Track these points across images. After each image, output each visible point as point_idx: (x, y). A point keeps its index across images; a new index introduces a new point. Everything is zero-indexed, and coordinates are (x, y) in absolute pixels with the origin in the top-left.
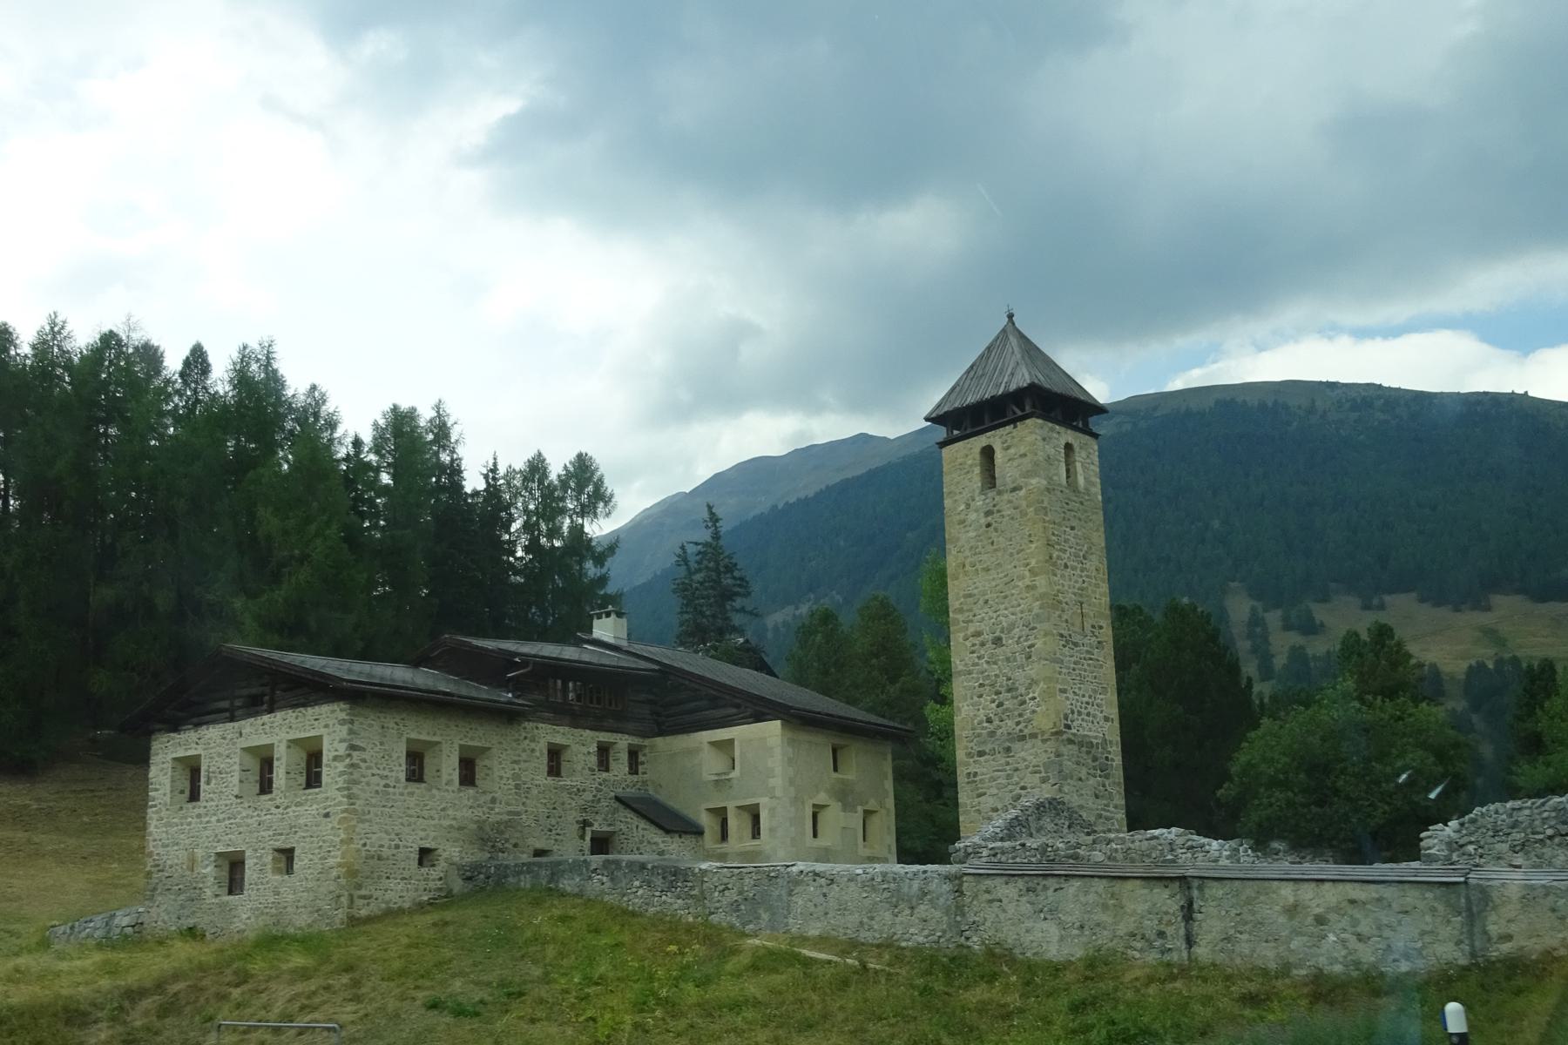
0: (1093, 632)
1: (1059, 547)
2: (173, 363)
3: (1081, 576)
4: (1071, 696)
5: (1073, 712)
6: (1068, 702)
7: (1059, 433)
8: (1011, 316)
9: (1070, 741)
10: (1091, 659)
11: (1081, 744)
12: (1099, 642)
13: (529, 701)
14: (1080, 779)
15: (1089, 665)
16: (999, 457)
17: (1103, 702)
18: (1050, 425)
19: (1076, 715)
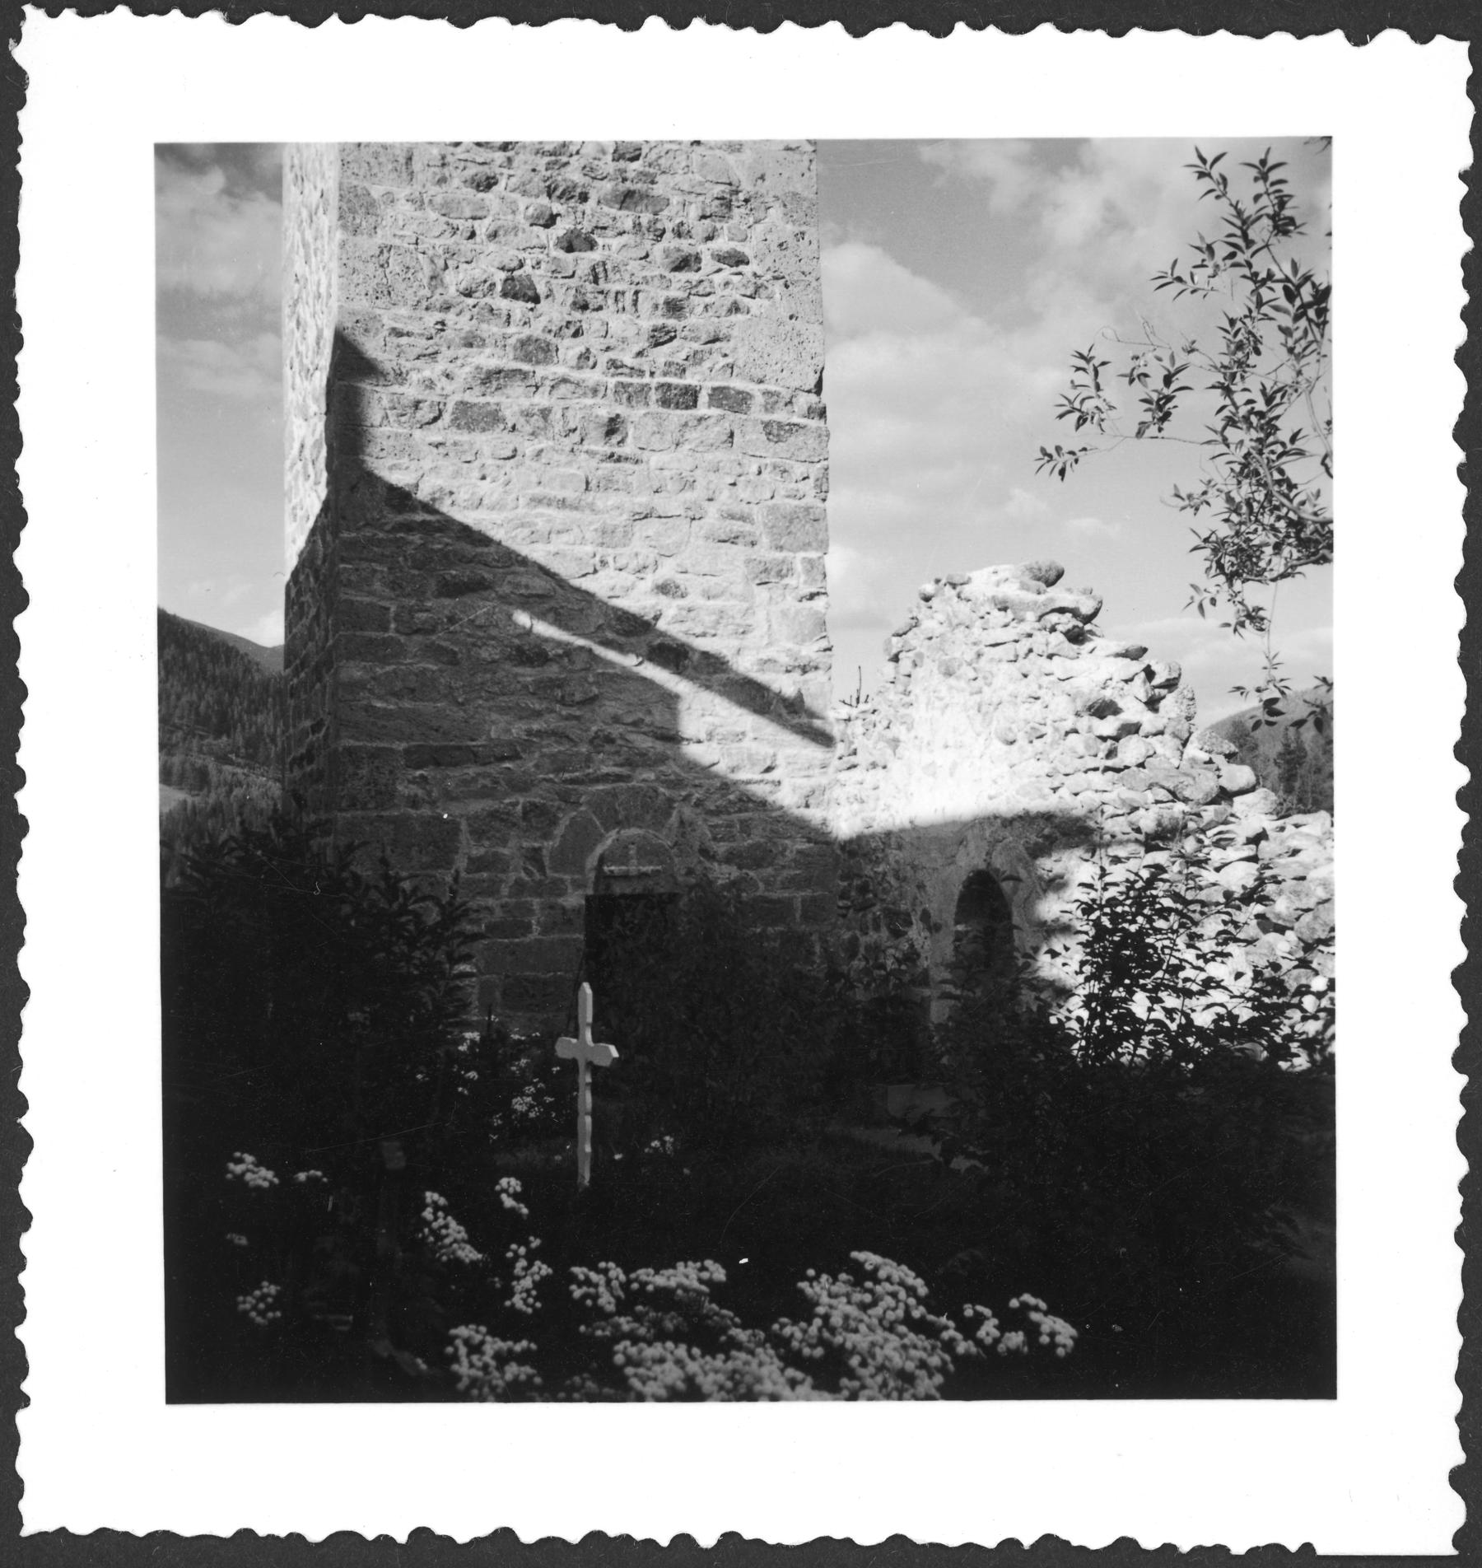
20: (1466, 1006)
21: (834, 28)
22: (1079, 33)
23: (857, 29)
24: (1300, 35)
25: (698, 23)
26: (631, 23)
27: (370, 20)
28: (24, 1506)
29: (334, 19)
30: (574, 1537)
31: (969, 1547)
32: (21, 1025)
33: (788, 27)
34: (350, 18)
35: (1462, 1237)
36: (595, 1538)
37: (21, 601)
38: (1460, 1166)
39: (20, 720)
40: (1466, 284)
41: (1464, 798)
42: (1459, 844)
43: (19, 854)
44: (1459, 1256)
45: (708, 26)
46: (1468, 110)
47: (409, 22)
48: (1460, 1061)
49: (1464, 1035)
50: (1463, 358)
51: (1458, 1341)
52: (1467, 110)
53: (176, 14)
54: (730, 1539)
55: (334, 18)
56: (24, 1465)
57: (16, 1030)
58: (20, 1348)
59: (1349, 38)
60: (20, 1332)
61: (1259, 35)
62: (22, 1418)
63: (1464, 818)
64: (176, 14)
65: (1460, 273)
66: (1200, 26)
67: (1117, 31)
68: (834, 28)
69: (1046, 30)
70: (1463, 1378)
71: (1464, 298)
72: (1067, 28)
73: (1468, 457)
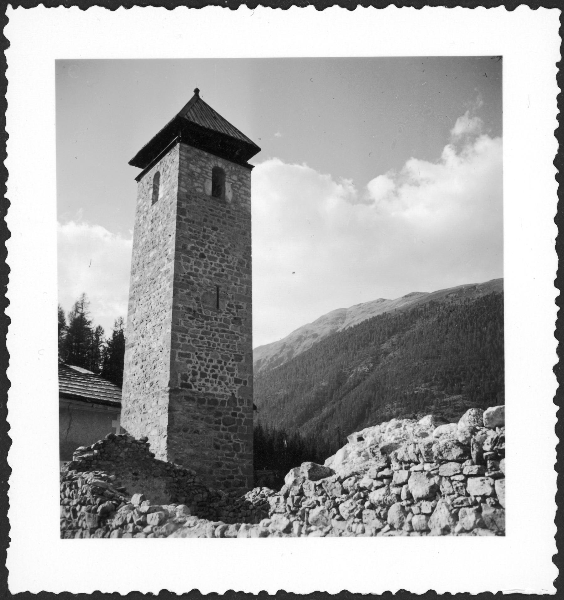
0: (230, 310)
1: (195, 241)
2: (107, 336)
3: (220, 266)
4: (195, 359)
5: (195, 374)
6: (189, 365)
7: (207, 158)
8: (197, 91)
9: (188, 399)
10: (224, 331)
11: (201, 401)
12: (235, 319)
13: (239, 490)
14: (197, 432)
15: (222, 336)
16: (161, 178)
17: (236, 367)
18: (197, 151)
19: (198, 377)
21: (204, 592)
22: (111, 592)
23: (320, 8)
25: (256, 593)
26: (8, 320)
27: (135, 8)
29: (394, 593)
30: (556, 420)
31: (559, 193)
33: (260, 7)
34: (388, 593)
36: (557, 334)
37: (556, 369)
39: (557, 323)
45: (149, 591)
47: (9, 405)
51: (555, 507)
53: (558, 111)
55: (394, 593)
57: (559, 206)
59: (7, 306)
64: (558, 111)
66: (451, 5)
67: (419, 7)
68: (7, 243)
72: (399, 6)
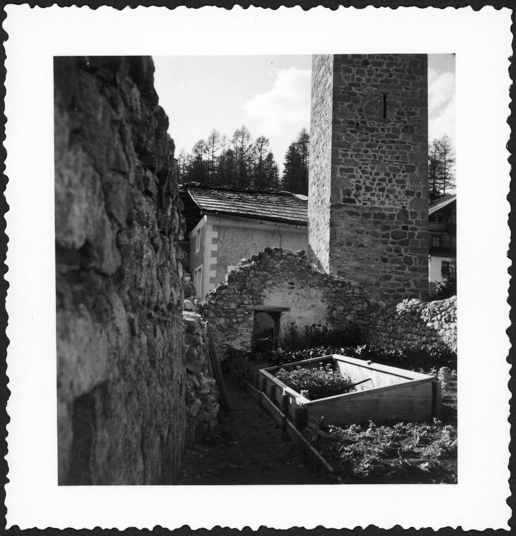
20: (4, 198)
24: (5, 57)
28: (7, 516)
30: (7, 231)
32: (6, 353)
35: (510, 420)
38: (6, 144)
40: (69, 6)
41: (247, 529)
42: (8, 254)
43: (6, 295)
44: (6, 113)
46: (511, 36)
48: (334, 8)
49: (5, 188)
50: (94, 7)
52: (510, 36)
54: (7, 285)
56: (7, 503)
58: (6, 462)
60: (6, 458)
61: (7, 324)
62: (7, 487)
63: (510, 277)
65: (9, 447)
69: (5, 144)
70: (511, 467)
71: (418, 528)
73: (436, 532)
